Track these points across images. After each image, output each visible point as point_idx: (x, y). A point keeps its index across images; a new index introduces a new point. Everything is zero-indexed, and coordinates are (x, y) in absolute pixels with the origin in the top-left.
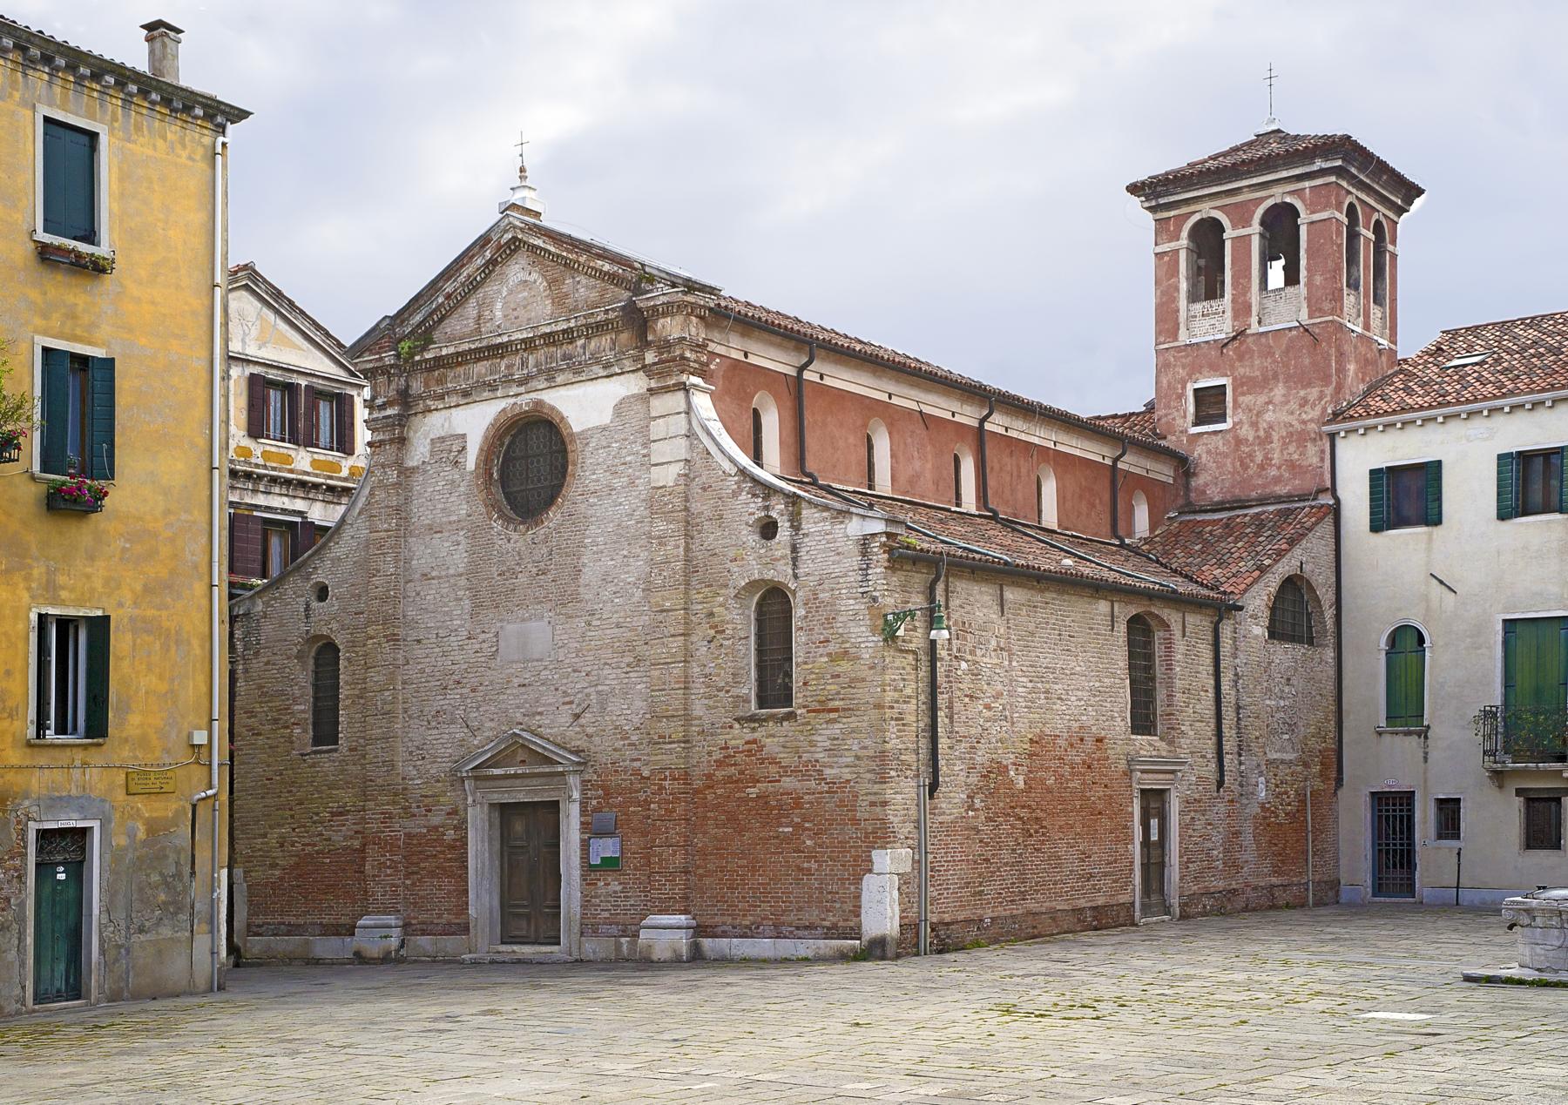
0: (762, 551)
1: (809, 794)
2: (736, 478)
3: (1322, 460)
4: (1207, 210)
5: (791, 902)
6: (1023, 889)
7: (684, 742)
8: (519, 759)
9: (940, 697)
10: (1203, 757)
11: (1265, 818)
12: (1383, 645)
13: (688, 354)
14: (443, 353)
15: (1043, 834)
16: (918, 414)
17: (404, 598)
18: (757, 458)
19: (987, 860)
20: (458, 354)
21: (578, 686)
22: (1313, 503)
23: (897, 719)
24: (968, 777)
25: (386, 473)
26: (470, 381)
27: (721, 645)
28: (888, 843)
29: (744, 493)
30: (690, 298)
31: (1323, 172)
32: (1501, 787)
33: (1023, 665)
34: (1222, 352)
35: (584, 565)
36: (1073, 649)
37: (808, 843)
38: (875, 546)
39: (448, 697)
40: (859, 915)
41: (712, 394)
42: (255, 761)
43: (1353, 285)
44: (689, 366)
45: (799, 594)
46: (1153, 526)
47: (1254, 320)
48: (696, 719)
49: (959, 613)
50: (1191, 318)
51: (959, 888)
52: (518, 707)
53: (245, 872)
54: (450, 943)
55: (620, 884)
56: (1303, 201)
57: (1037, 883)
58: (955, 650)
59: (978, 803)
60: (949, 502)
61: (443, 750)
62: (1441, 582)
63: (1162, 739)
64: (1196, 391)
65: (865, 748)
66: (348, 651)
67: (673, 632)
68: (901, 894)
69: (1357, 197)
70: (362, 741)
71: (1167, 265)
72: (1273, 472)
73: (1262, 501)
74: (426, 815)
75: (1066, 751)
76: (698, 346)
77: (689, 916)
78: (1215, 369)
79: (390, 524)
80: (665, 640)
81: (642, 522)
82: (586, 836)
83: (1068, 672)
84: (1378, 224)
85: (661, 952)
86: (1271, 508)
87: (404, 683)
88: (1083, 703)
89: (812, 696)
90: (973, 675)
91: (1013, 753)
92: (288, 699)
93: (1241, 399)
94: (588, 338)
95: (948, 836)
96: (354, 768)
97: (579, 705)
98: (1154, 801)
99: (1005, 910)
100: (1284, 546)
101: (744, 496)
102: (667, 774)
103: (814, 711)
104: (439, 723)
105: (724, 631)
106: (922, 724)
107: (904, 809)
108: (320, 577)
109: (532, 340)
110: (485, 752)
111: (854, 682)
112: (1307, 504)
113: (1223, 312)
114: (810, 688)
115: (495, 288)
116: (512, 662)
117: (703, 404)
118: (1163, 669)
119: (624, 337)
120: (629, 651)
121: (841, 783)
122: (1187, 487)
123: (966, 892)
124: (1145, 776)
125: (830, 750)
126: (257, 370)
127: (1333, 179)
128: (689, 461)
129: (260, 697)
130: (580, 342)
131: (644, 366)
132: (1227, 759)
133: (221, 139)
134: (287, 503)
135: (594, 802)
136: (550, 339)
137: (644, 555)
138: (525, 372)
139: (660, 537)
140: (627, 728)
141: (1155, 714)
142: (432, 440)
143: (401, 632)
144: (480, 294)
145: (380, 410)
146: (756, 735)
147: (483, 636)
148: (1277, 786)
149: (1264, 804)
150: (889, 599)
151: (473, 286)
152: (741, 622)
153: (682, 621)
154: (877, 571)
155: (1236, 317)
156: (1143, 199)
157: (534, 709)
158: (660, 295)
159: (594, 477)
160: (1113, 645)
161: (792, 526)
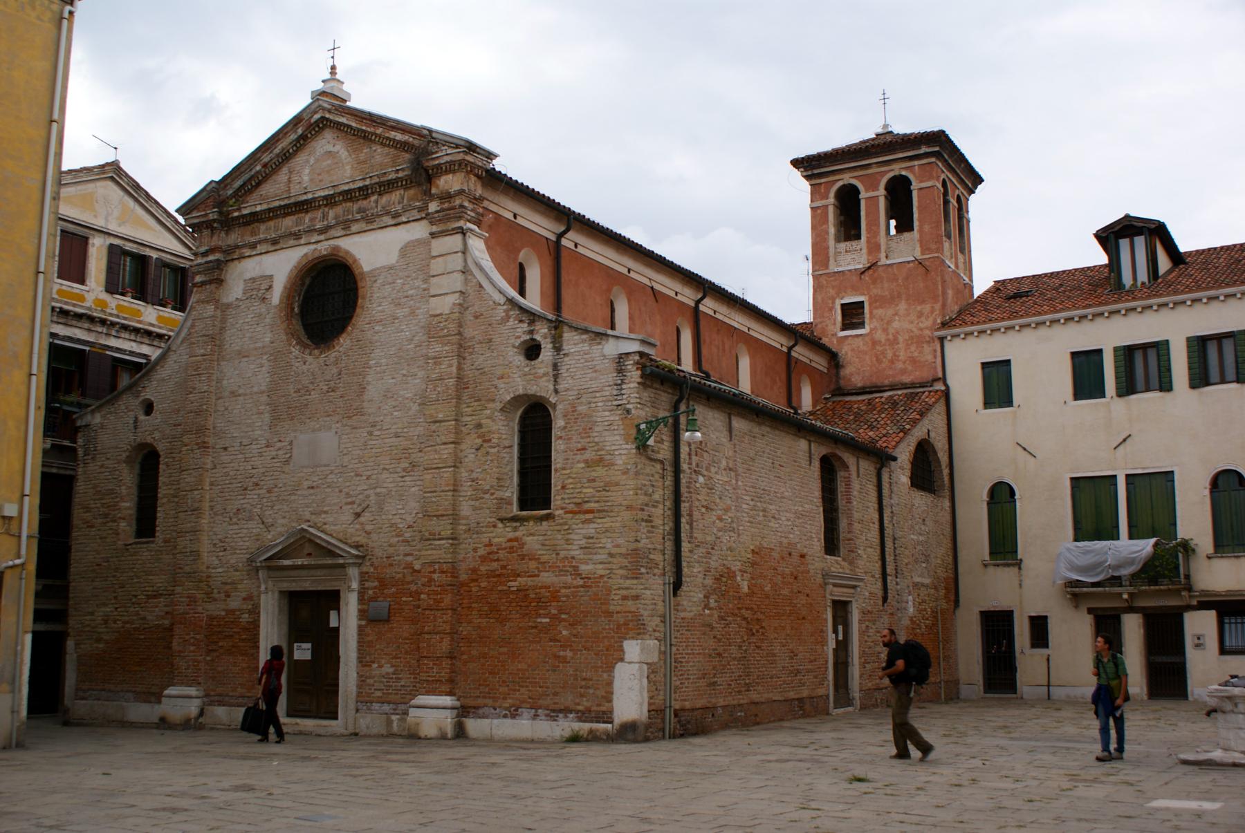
0: (527, 369)
1: (565, 588)
2: (505, 307)
4: (847, 179)
5: (547, 688)
6: (747, 681)
7: (452, 539)
8: (306, 551)
9: (683, 505)
11: (913, 629)
12: (985, 497)
13: (466, 204)
15: (763, 634)
16: (650, 289)
17: (215, 412)
18: (522, 292)
19: (719, 655)
20: (270, 210)
22: (931, 389)
23: (647, 521)
24: (704, 579)
26: (279, 232)
27: (487, 453)
28: (639, 634)
29: (511, 320)
30: (469, 158)
31: (927, 155)
32: (1076, 607)
33: (746, 485)
34: (861, 278)
35: (368, 383)
38: (629, 363)
39: (248, 496)
40: (610, 701)
41: (487, 242)
43: (949, 237)
44: (466, 213)
45: (560, 407)
46: (815, 403)
47: (883, 255)
48: (463, 519)
50: (837, 253)
51: (697, 678)
52: (307, 507)
53: (76, 644)
56: (914, 174)
57: (758, 676)
58: (694, 464)
59: (712, 603)
61: (241, 543)
62: (1025, 449)
63: (844, 560)
65: (618, 546)
66: (166, 457)
67: (444, 441)
68: (649, 682)
70: (174, 534)
71: (817, 214)
72: (900, 365)
73: (893, 387)
74: (225, 600)
76: (475, 199)
77: (453, 698)
78: (856, 290)
79: (206, 349)
80: (437, 447)
82: (363, 623)
84: (958, 197)
85: (428, 730)
86: (900, 392)
87: (212, 484)
88: (790, 523)
89: (569, 498)
90: (708, 488)
91: (740, 561)
92: (117, 497)
93: (875, 312)
94: (380, 194)
95: (689, 630)
96: (167, 557)
97: (360, 505)
98: (841, 609)
99: (734, 700)
100: (918, 417)
101: (512, 322)
103: (571, 512)
104: (239, 520)
105: (490, 440)
106: (667, 528)
107: (652, 604)
108: (148, 394)
113: (861, 250)
114: (567, 491)
115: (304, 158)
116: (303, 467)
117: (477, 246)
118: (844, 502)
120: (406, 458)
121: (595, 578)
122: (837, 375)
123: (702, 683)
125: (586, 548)
126: (117, 242)
127: (933, 160)
128: (463, 293)
129: (94, 495)
131: (428, 214)
133: (68, 8)
134: (134, 347)
136: (349, 196)
137: (421, 374)
138: (325, 223)
139: (435, 358)
140: (401, 526)
143: (211, 441)
145: (203, 256)
146: (518, 534)
147: (279, 444)
148: (920, 604)
149: (912, 617)
150: (641, 412)
151: (286, 157)
152: (506, 432)
153: (454, 431)
155: (870, 252)
156: (802, 170)
157: (321, 508)
158: (444, 155)
159: (380, 308)
160: (811, 477)
161: (554, 348)
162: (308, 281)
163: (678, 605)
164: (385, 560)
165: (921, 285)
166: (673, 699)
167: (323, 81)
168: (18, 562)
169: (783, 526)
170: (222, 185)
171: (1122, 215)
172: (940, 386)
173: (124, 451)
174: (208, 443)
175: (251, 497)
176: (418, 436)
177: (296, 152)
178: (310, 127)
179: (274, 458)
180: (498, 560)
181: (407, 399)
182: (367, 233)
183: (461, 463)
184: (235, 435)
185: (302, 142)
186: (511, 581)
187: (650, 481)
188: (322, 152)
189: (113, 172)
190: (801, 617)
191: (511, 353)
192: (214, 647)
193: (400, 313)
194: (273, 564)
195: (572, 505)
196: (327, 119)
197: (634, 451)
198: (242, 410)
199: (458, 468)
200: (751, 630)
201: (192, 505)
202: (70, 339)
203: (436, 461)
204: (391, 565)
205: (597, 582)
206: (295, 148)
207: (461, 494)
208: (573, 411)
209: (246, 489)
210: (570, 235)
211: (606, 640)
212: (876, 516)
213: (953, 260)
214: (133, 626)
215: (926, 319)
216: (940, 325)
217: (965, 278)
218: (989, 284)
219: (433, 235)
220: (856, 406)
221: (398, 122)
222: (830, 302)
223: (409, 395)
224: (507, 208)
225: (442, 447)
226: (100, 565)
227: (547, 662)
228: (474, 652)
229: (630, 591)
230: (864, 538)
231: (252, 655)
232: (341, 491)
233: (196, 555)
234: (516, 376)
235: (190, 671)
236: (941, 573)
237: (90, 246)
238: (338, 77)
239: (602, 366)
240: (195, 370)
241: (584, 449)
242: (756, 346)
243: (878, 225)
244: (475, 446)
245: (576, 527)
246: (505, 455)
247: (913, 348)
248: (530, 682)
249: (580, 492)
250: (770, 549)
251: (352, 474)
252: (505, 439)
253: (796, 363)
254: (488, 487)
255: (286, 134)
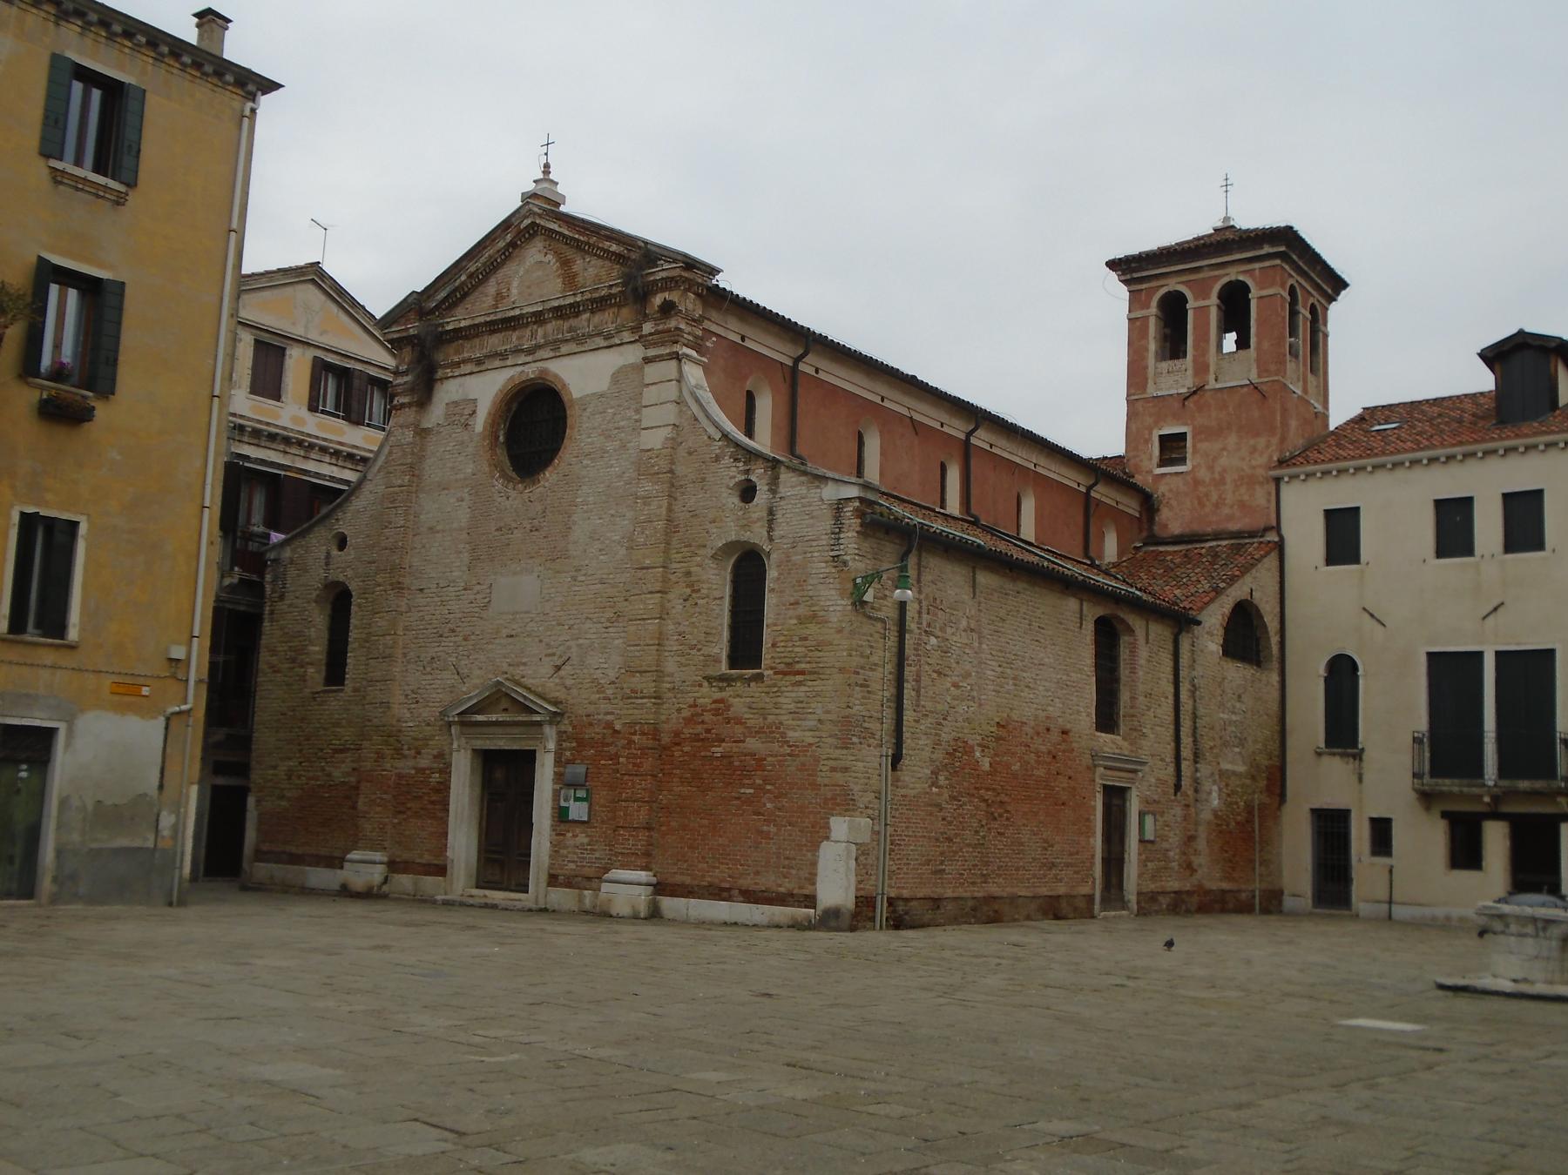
1: (771, 756)
2: (720, 443)
3: (1269, 501)
4: (1173, 285)
6: (985, 872)
7: (655, 698)
9: (907, 669)
10: (1162, 760)
11: (1218, 825)
13: (682, 326)
14: (462, 326)
15: (1008, 819)
16: (908, 420)
18: (749, 433)
19: (949, 840)
21: (561, 638)
22: (1261, 540)
23: (862, 686)
24: (933, 753)
25: (403, 434)
26: (485, 351)
27: (696, 604)
28: (847, 810)
32: (1428, 809)
34: (1184, 404)
36: (1042, 641)
37: (769, 805)
40: (814, 884)
42: (273, 696)
44: (683, 337)
45: (774, 556)
46: (1121, 553)
48: (668, 676)
49: (930, 589)
50: (1158, 374)
51: (919, 864)
52: (505, 657)
54: (429, 883)
55: (587, 836)
56: (1254, 280)
59: (942, 780)
60: (934, 503)
61: (434, 696)
62: (1372, 615)
63: (1124, 739)
64: (1161, 437)
65: (828, 712)
67: (650, 589)
69: (1297, 281)
70: (364, 683)
71: (1136, 327)
72: (1226, 511)
75: (1032, 738)
76: (694, 320)
77: (651, 873)
78: (1177, 418)
81: (630, 483)
82: (558, 787)
83: (1036, 662)
85: (621, 907)
86: (1224, 543)
87: (406, 629)
88: (1050, 694)
89: (780, 658)
92: (305, 640)
93: (1199, 445)
94: (593, 312)
95: (910, 810)
97: (561, 657)
99: (966, 891)
100: (1237, 573)
101: (727, 461)
102: (637, 728)
104: (433, 669)
105: (699, 590)
106: (886, 694)
107: (865, 778)
109: (540, 313)
110: (470, 699)
111: (819, 647)
112: (1255, 540)
113: (1186, 370)
114: (778, 650)
115: (513, 268)
117: (694, 374)
118: (1127, 672)
119: (625, 311)
124: (1109, 773)
125: (795, 713)
126: (320, 354)
127: (1278, 262)
128: (678, 427)
130: (586, 316)
132: (1184, 765)
133: (250, 105)
135: (568, 753)
136: (560, 313)
137: (630, 514)
138: (533, 342)
139: (644, 498)
141: (1118, 714)
142: (447, 404)
143: (407, 581)
144: (501, 274)
146: (723, 694)
147: (478, 587)
148: (1229, 795)
149: (1217, 811)
151: (493, 267)
152: (718, 583)
153: (661, 579)
154: (850, 536)
156: (1120, 273)
159: (589, 440)
162: (514, 407)
163: (898, 780)
164: (585, 718)
165: (1256, 414)
166: (886, 885)
167: (535, 181)
168: (184, 707)
169: (1040, 697)
170: (425, 297)
171: (1514, 331)
172: (1272, 537)
173: (315, 590)
174: (403, 583)
175: (446, 644)
176: (624, 583)
177: (504, 262)
178: (519, 233)
179: (472, 603)
180: (703, 722)
181: (614, 541)
182: (577, 356)
183: (668, 614)
184: (431, 576)
185: (510, 250)
186: (716, 746)
187: (869, 641)
188: (532, 262)
189: (313, 275)
190: (1061, 802)
191: (725, 495)
192: (402, 809)
193: (610, 446)
194: (465, 722)
195: (783, 665)
196: (538, 225)
197: (850, 608)
198: (440, 548)
199: (664, 619)
200: (992, 814)
201: (384, 652)
202: (263, 462)
203: (641, 612)
204: (591, 724)
205: (806, 751)
206: (503, 257)
207: (666, 648)
208: (787, 561)
209: (441, 636)
210: (809, 358)
211: (811, 816)
212: (1171, 689)
213: (1301, 383)
214: (319, 783)
215: (1257, 454)
216: (1277, 463)
217: (1316, 405)
218: (1355, 411)
219: (647, 360)
220: (1169, 558)
221: (612, 230)
222: (1146, 432)
223: (616, 538)
224: (732, 329)
225: (649, 596)
226: (285, 714)
227: (750, 838)
228: (674, 824)
229: (839, 762)
230: (1153, 715)
231: (442, 818)
232: (541, 641)
233: (387, 705)
234: (728, 519)
235: (374, 834)
236: (1264, 761)
237: (287, 357)
238: (551, 177)
239: (819, 512)
240: (392, 502)
241: (797, 603)
242: (1042, 484)
243: (1207, 341)
244: (685, 597)
245: (785, 689)
246: (714, 607)
247: (1243, 490)
248: (730, 859)
249: (792, 651)
250: (1022, 723)
251: (554, 623)
252: (716, 589)
253: (1097, 505)
254: (695, 642)
255: (494, 240)
